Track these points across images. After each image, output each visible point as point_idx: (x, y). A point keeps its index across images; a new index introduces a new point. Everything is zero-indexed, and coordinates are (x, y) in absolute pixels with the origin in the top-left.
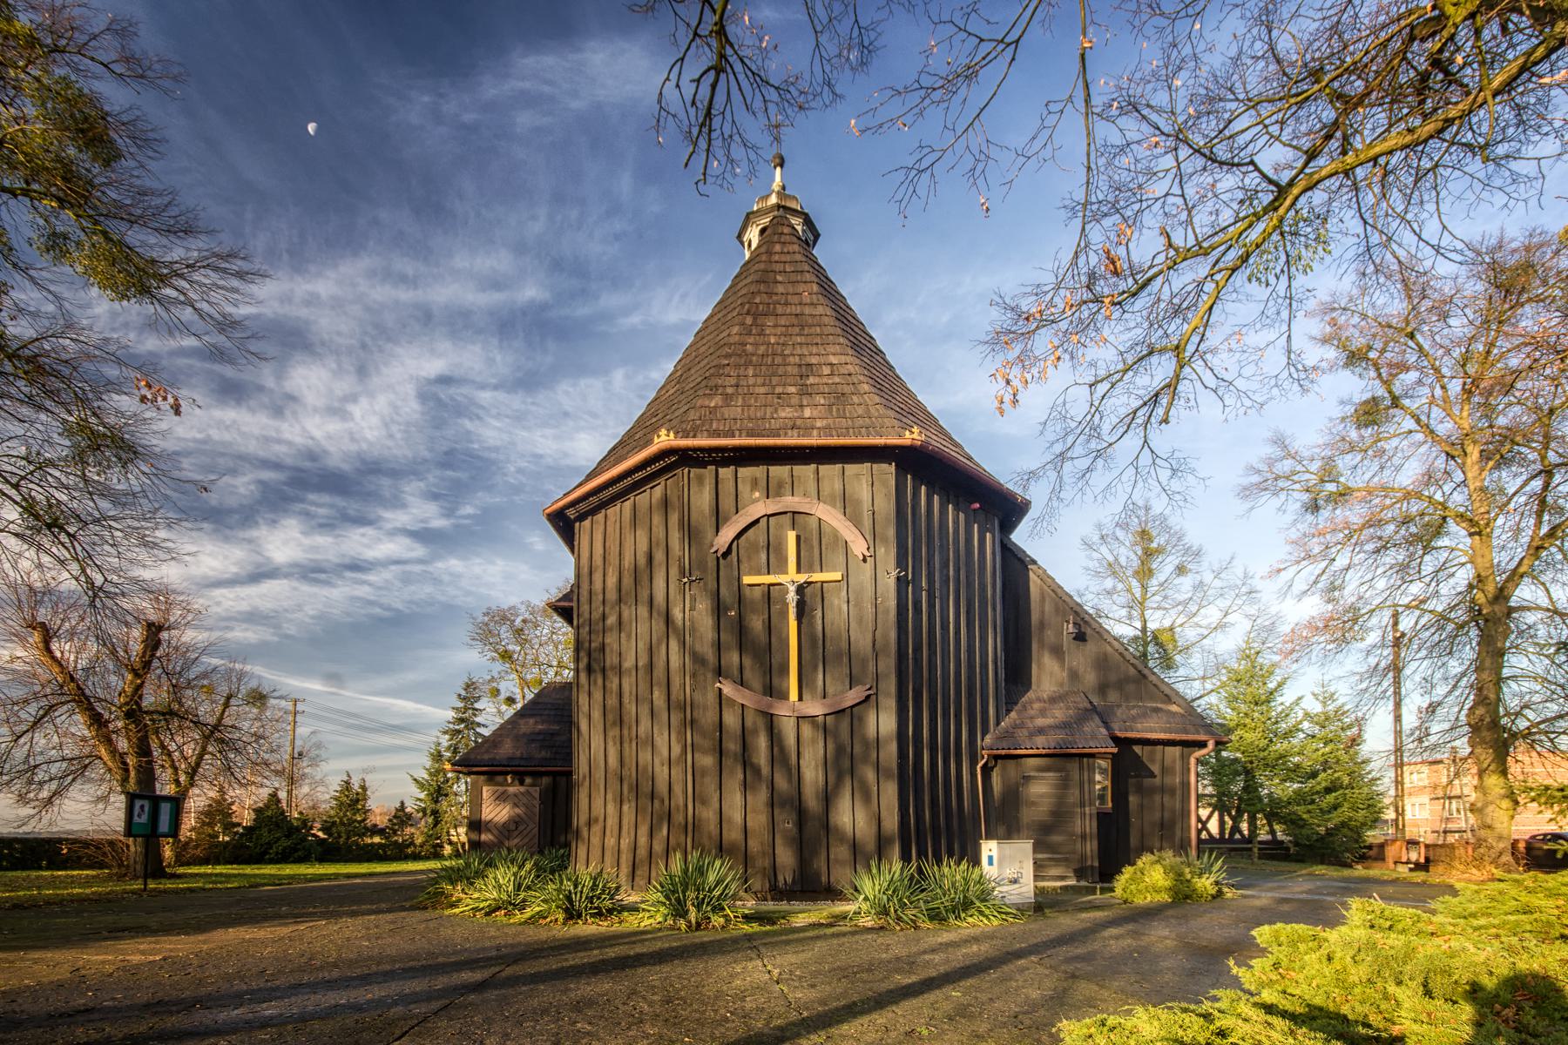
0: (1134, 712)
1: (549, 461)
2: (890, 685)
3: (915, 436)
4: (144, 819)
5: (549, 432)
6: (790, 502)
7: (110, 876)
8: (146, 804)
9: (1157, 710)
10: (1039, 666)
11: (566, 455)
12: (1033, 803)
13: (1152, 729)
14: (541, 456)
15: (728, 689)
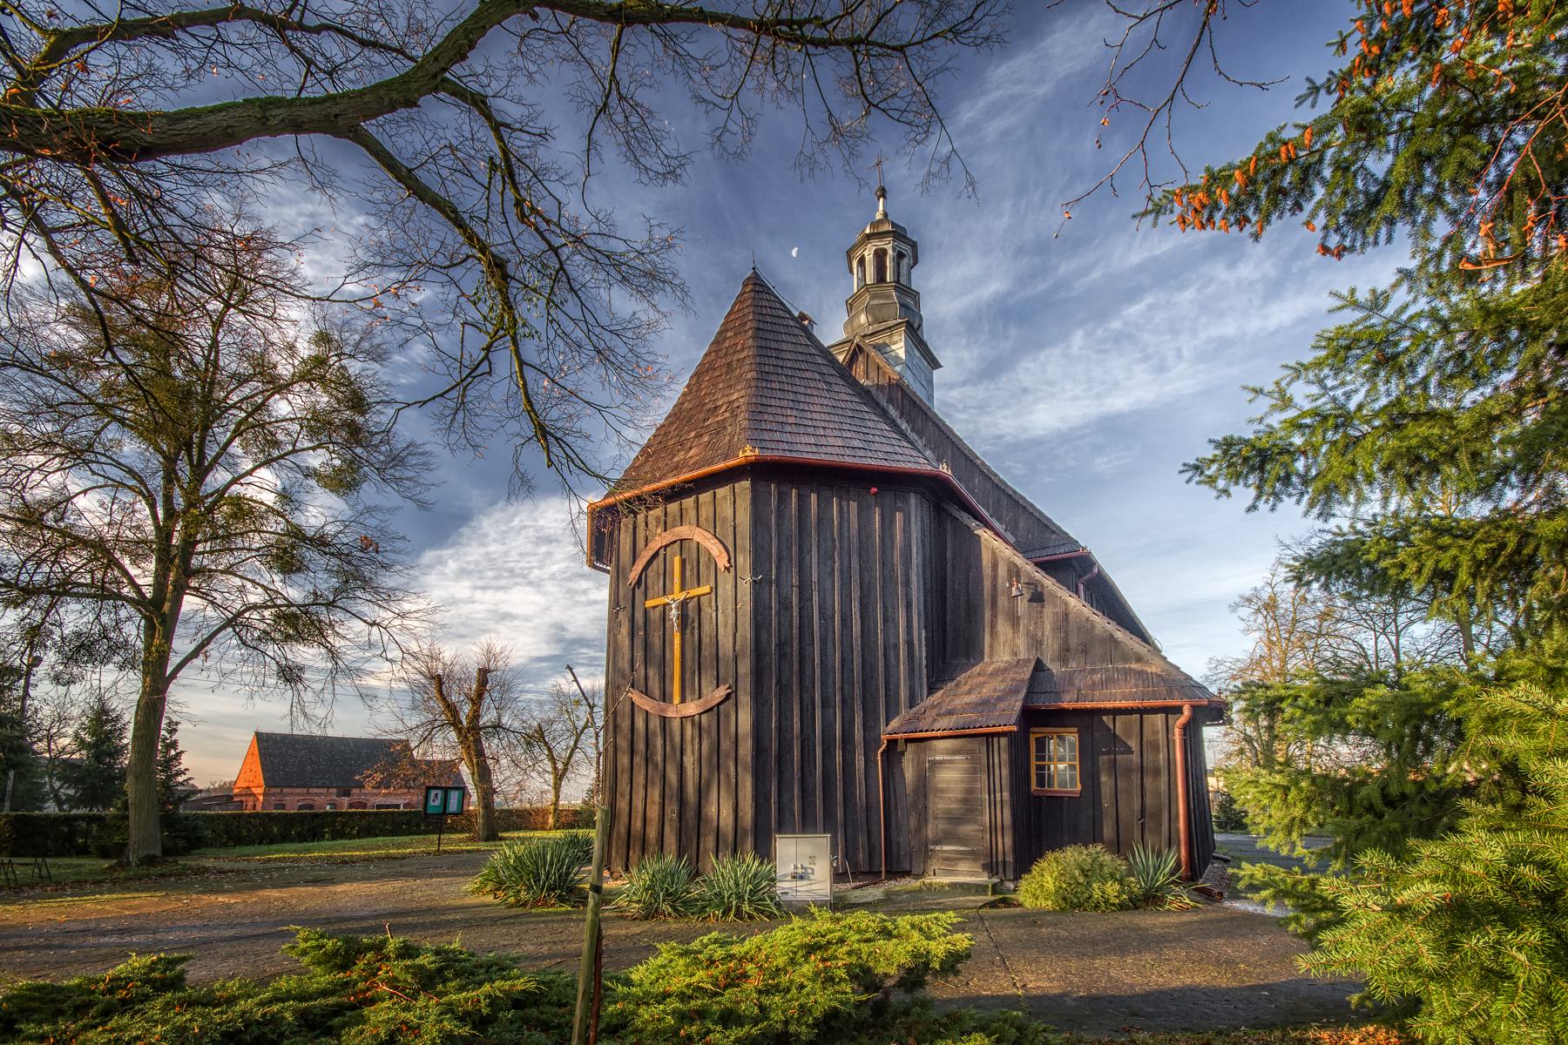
0: (1097, 677)
1: (1009, 439)
2: (746, 686)
3: (748, 453)
4: (438, 803)
5: (1007, 412)
6: (683, 531)
7: (470, 839)
8: (439, 792)
9: (1128, 672)
10: (994, 633)
11: (1025, 429)
12: (942, 791)
13: (1118, 697)
14: (1001, 437)
15: (637, 697)
